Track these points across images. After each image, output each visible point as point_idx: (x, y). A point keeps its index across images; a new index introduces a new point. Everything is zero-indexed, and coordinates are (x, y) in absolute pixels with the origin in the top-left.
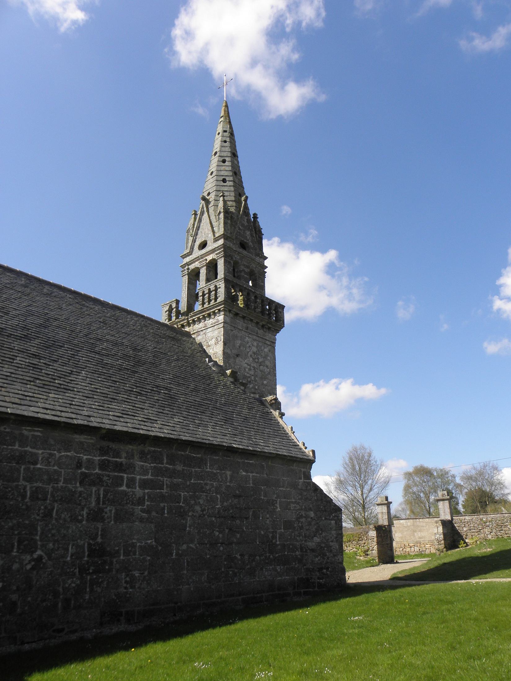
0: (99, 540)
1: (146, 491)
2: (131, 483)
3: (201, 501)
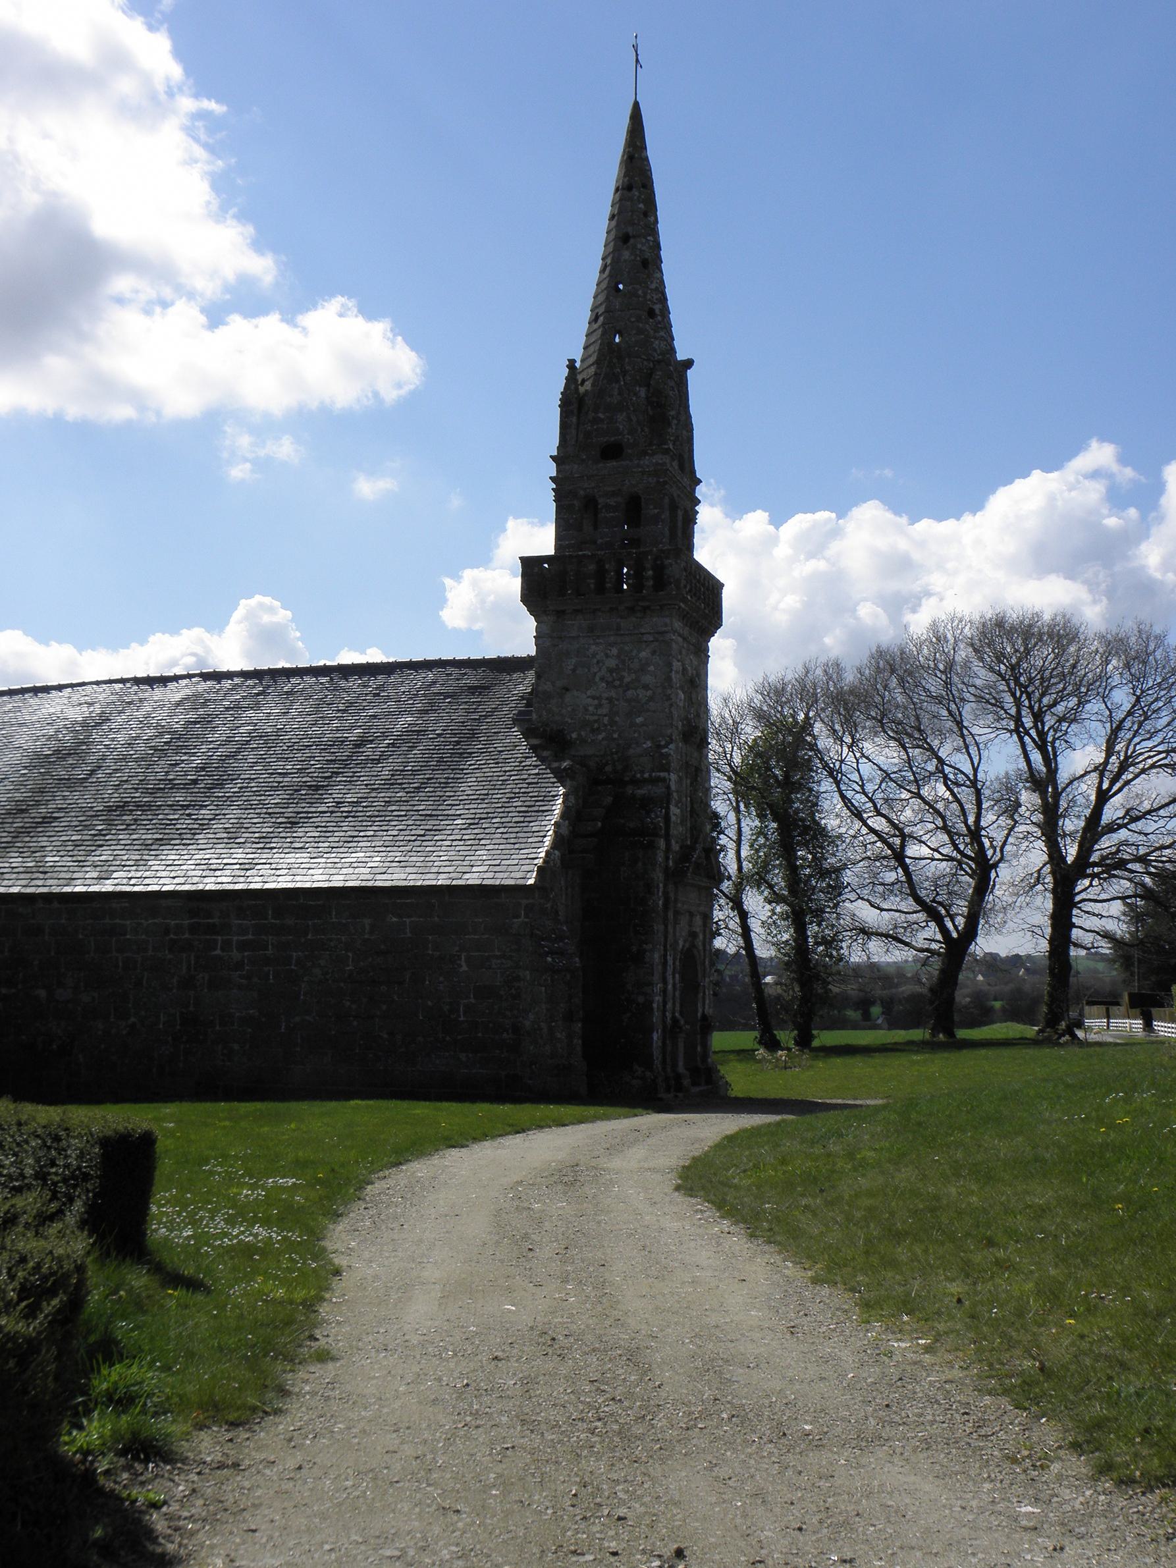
0: (191, 1008)
1: (246, 954)
2: (227, 945)
3: (322, 962)
